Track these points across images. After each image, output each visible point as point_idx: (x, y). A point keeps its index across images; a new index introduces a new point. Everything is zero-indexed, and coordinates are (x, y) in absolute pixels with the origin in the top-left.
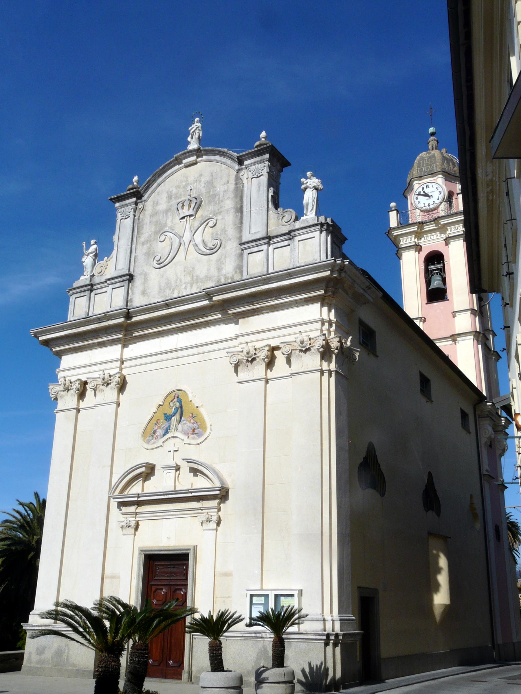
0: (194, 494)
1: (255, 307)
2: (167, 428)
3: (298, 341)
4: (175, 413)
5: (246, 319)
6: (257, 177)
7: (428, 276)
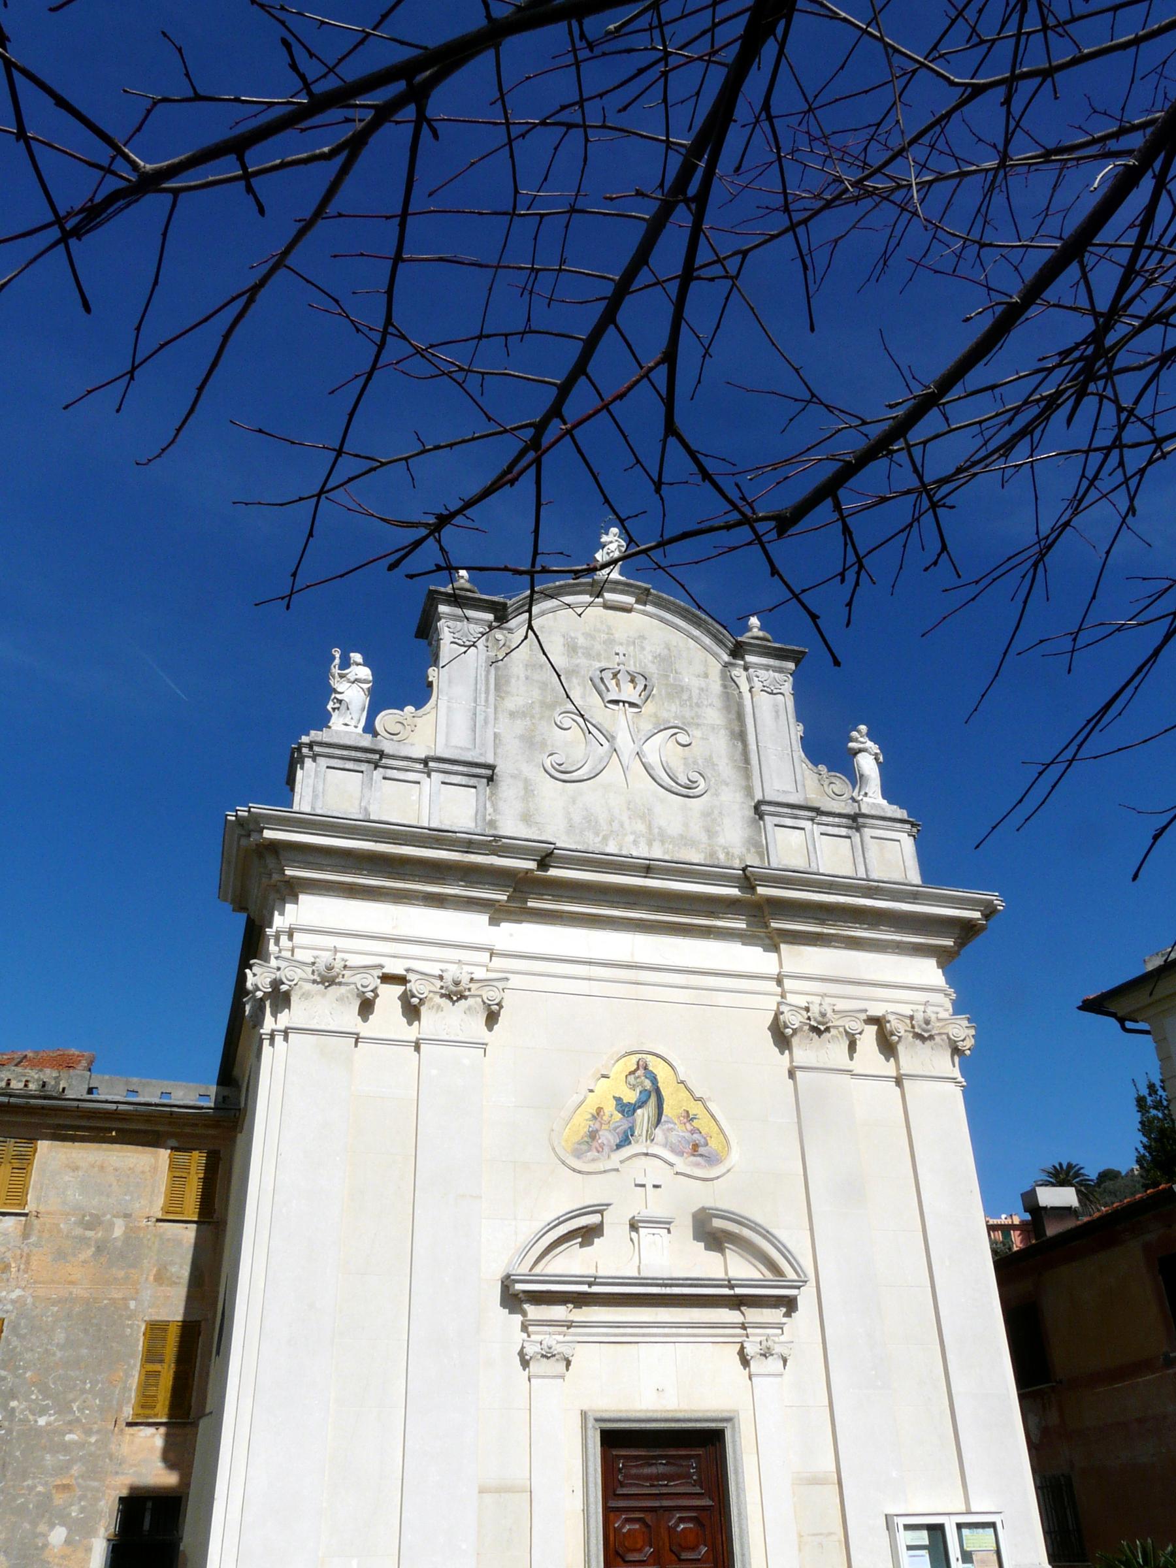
1: (825, 931)
2: (625, 1132)
5: (796, 947)
6: (772, 693)
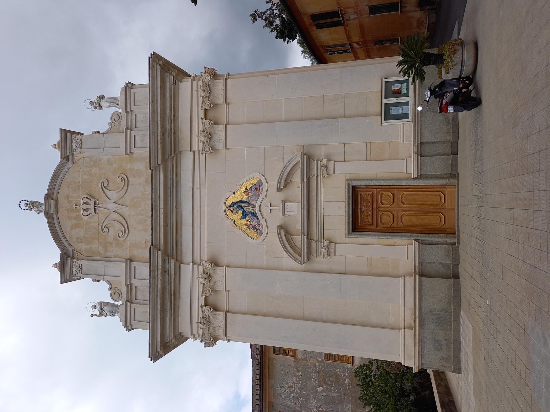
0: (305, 180)
3: (203, 282)
4: (242, 208)
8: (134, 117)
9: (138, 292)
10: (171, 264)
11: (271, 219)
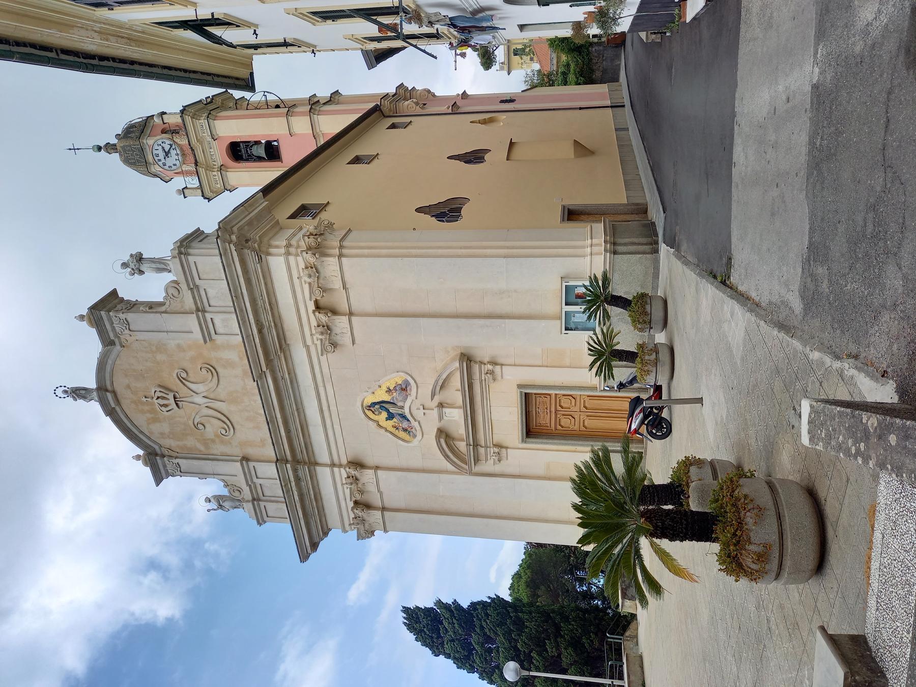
3: (308, 280)
7: (251, 158)
8: (203, 293)
9: (264, 488)
10: (304, 471)
11: (428, 424)
